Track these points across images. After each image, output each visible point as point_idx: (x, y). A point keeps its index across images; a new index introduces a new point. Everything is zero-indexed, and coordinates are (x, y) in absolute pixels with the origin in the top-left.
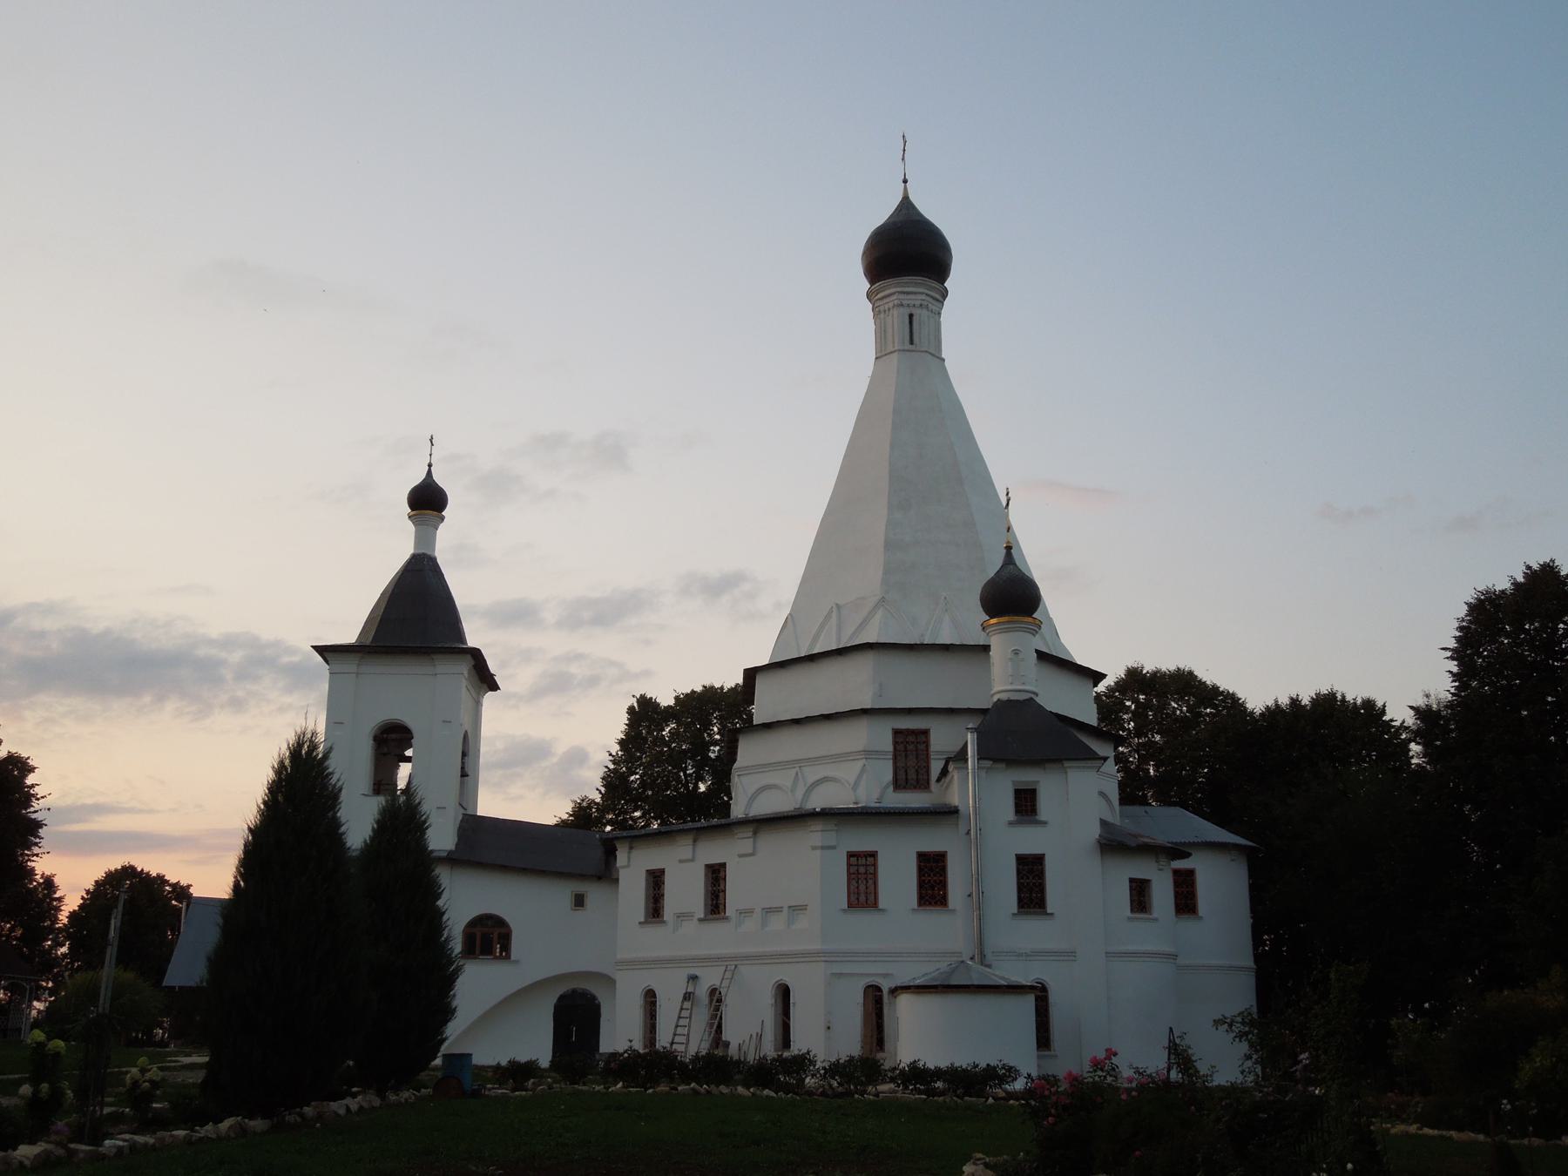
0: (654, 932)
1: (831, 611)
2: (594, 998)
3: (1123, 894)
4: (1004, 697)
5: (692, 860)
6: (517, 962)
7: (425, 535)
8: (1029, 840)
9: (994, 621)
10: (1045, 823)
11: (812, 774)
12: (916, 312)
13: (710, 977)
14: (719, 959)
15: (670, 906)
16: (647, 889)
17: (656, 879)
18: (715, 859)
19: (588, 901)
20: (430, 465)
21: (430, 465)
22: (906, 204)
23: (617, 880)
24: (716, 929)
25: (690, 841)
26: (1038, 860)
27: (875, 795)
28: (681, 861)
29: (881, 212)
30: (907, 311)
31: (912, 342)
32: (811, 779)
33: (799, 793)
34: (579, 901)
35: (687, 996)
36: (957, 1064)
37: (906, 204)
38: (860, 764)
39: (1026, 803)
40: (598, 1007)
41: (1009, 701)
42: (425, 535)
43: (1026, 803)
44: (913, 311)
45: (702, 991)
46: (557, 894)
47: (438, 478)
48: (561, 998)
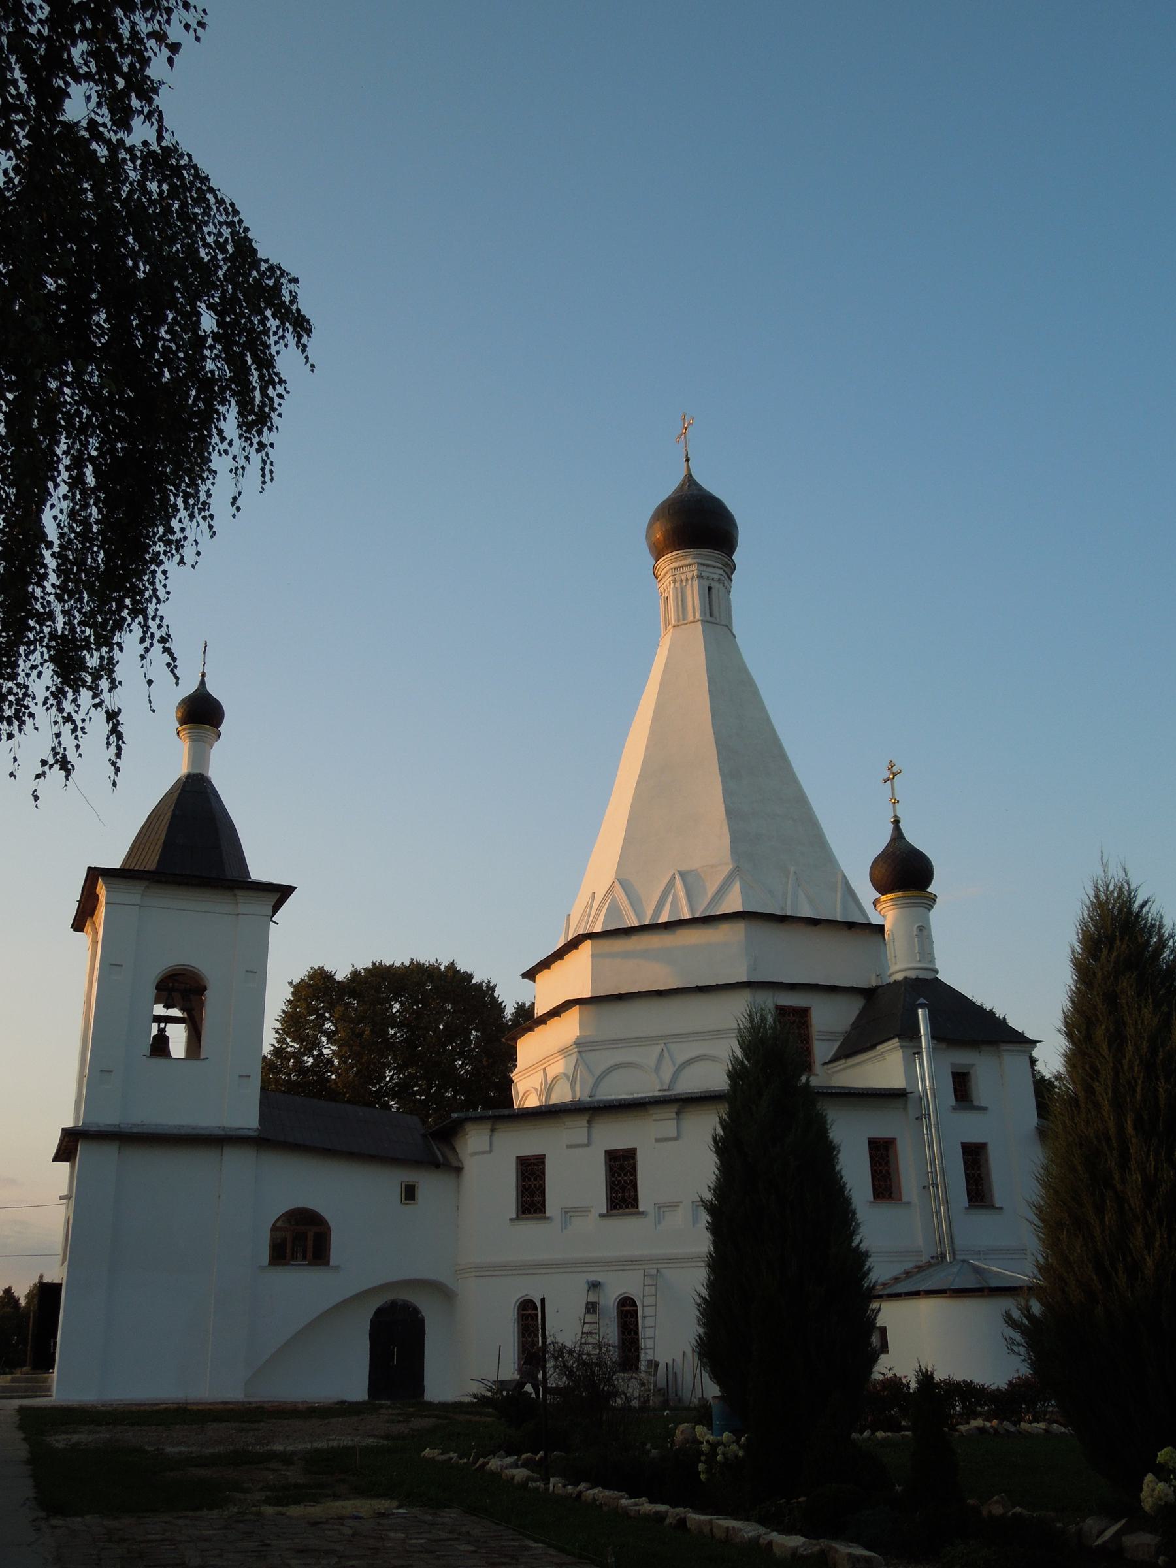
0: (531, 1229)
1: (672, 882)
2: (416, 1311)
3: (396, 1193)
4: (912, 975)
5: (588, 1145)
6: (337, 1268)
7: (199, 755)
8: (971, 1127)
9: (883, 898)
10: (984, 1109)
11: (684, 1052)
12: (714, 585)
13: (616, 1286)
14: (633, 1261)
15: (554, 1200)
16: (988, 1174)
17: (531, 1174)
18: (620, 1143)
19: (420, 1194)
20: (203, 675)
21: (203, 675)
22: (689, 479)
23: (458, 1170)
24: (625, 1225)
25: (585, 1123)
26: (540, 1161)
27: (587, 1092)
28: (569, 1146)
29: (666, 487)
30: (706, 583)
31: (711, 615)
32: (680, 1060)
33: (667, 1073)
34: (410, 1193)
35: (591, 1308)
36: (976, 1381)
37: (689, 479)
38: (658, 1049)
39: (962, 1084)
40: (422, 1321)
41: (917, 979)
42: (199, 755)
43: (962, 1084)
44: (713, 584)
45: (609, 1299)
46: (383, 1184)
47: (213, 689)
48: (379, 1312)
